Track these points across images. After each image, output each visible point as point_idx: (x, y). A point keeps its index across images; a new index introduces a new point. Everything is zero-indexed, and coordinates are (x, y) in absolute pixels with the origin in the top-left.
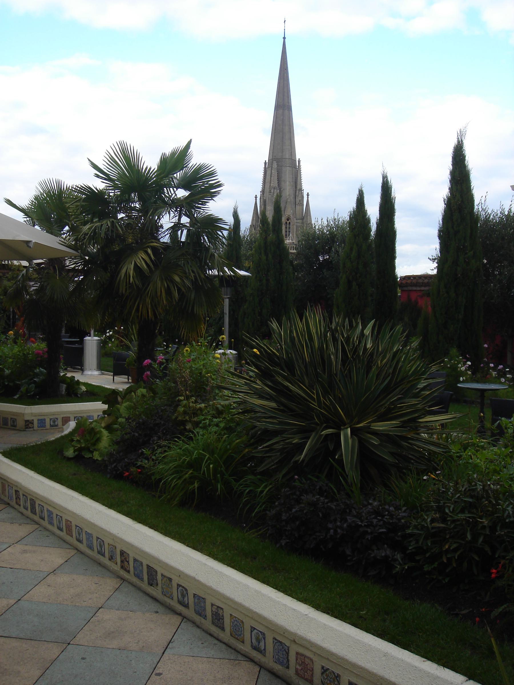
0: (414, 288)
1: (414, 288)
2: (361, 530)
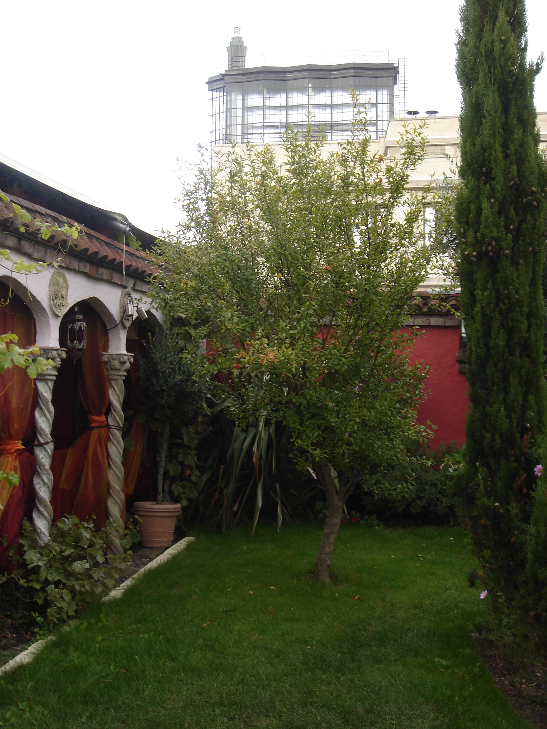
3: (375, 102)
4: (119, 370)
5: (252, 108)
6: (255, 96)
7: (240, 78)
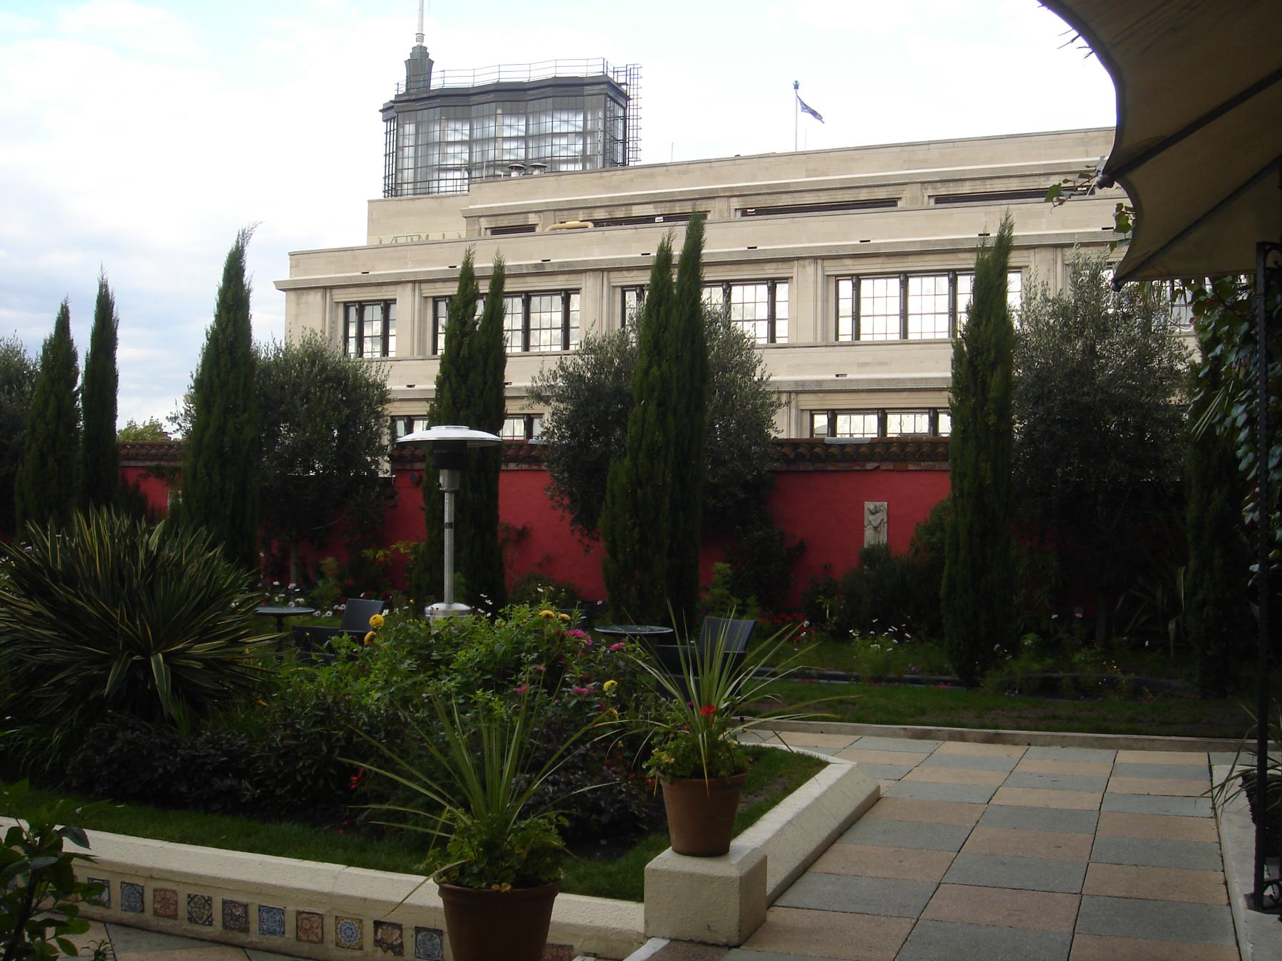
0: (133, 463)
1: (133, 463)
2: (199, 761)
7: (422, 101)
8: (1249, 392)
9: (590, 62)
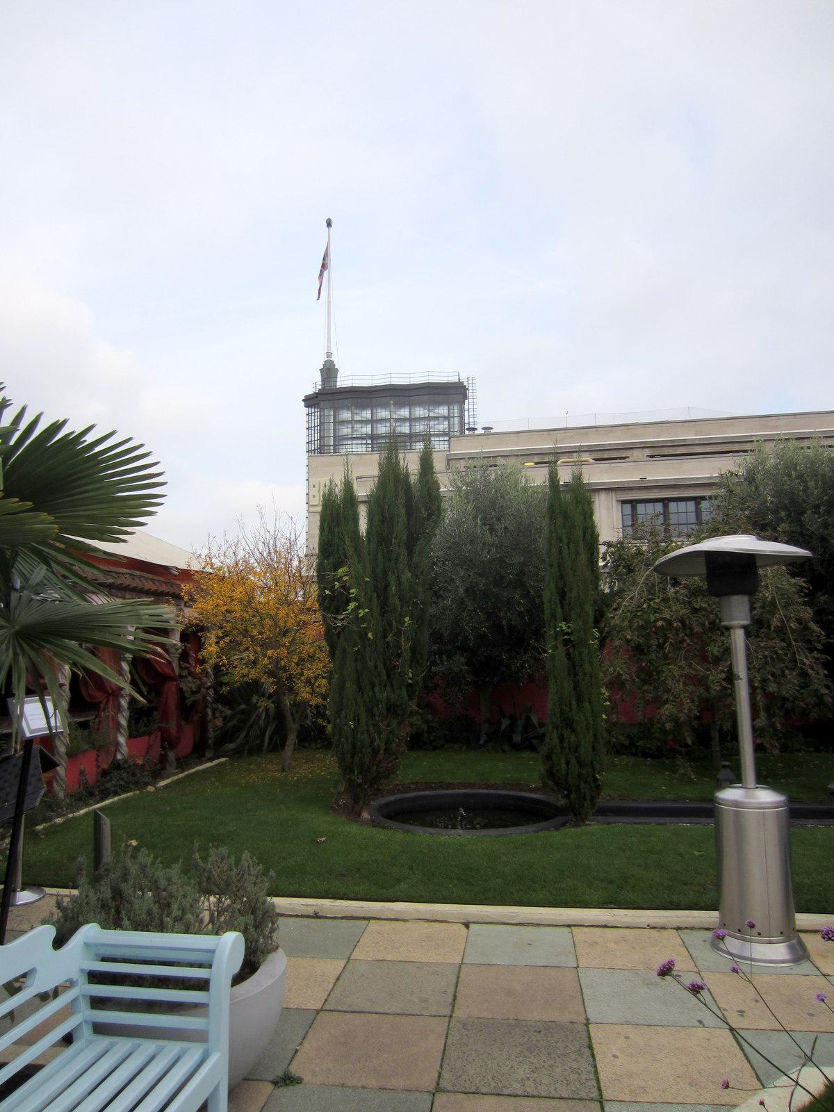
3: (447, 415)
4: (174, 654)
5: (343, 422)
6: (345, 412)
7: (329, 398)
8: (146, 693)
9: (412, 376)
